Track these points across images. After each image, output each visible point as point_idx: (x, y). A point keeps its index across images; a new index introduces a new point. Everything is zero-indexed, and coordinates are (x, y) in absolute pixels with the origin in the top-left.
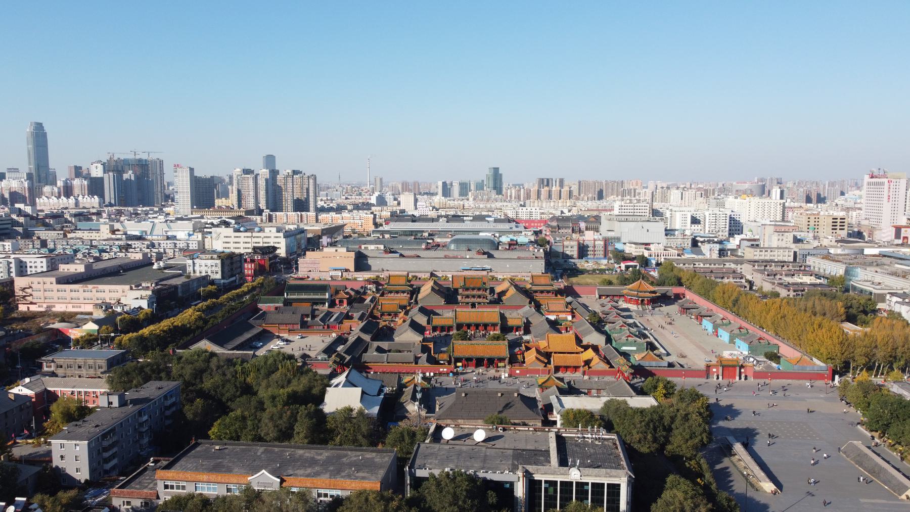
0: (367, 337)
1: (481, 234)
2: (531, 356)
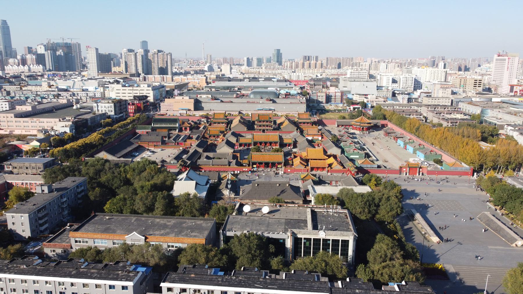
0: (200, 150)
1: (269, 89)
2: (297, 161)
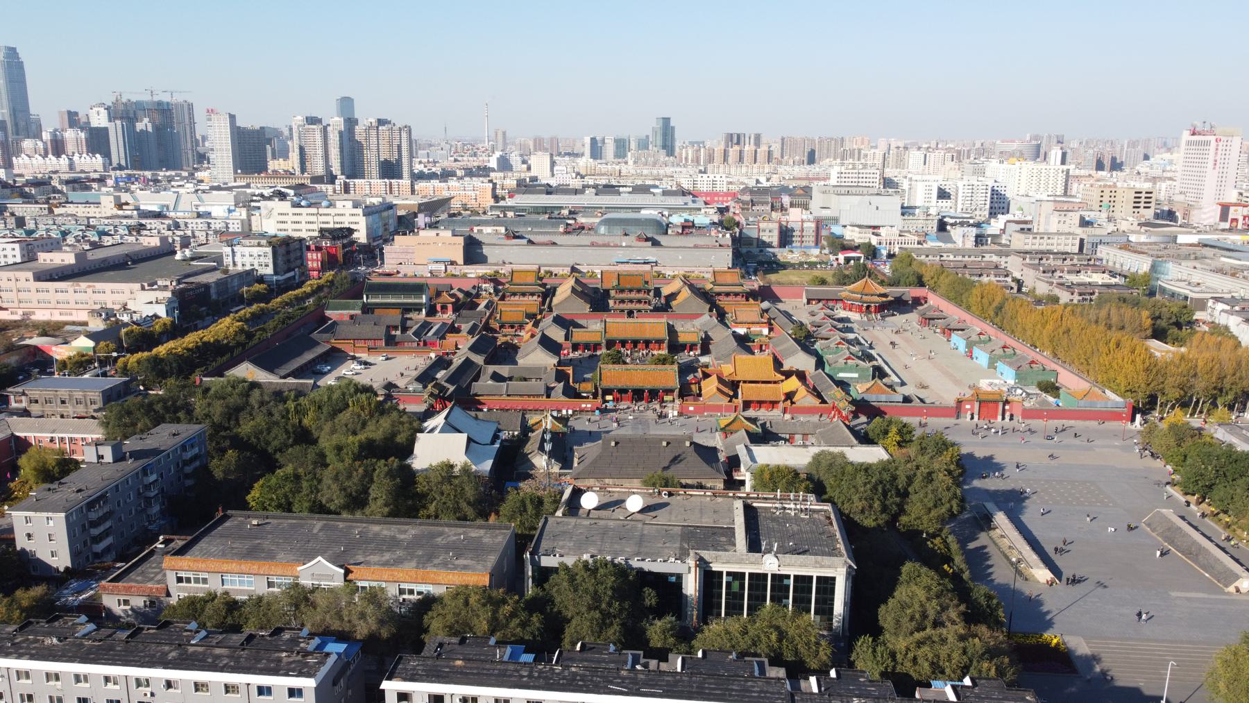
0: (479, 359)
1: (643, 212)
2: (710, 386)
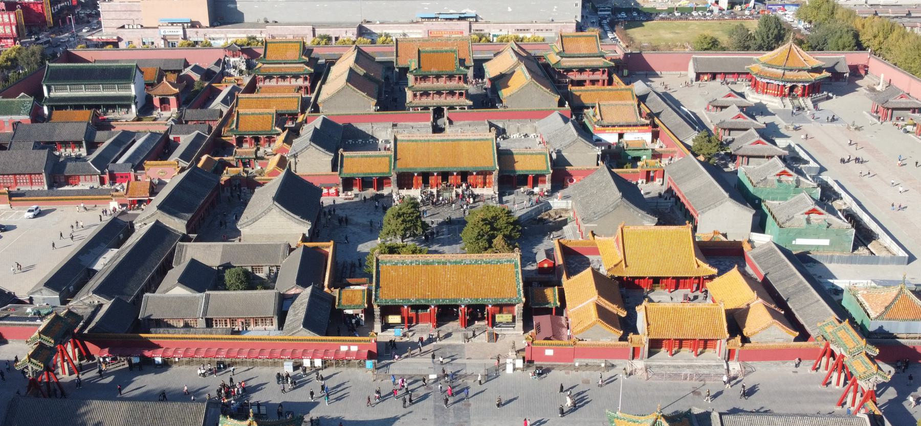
0: (178, 225)
2: (581, 295)
